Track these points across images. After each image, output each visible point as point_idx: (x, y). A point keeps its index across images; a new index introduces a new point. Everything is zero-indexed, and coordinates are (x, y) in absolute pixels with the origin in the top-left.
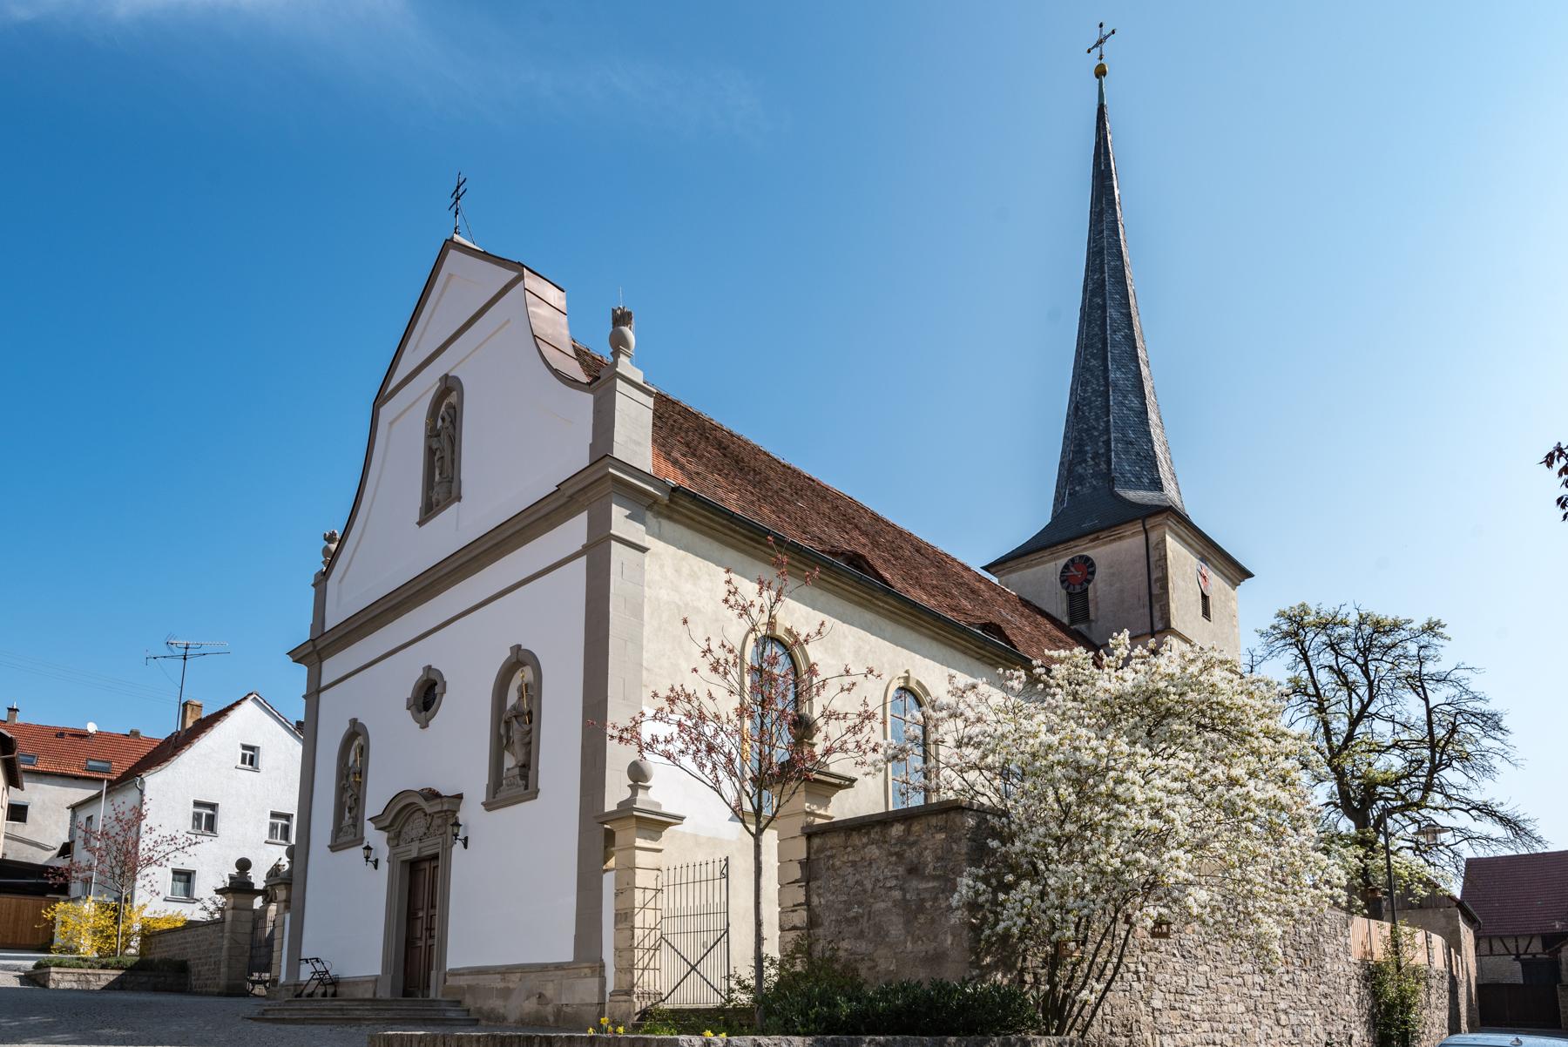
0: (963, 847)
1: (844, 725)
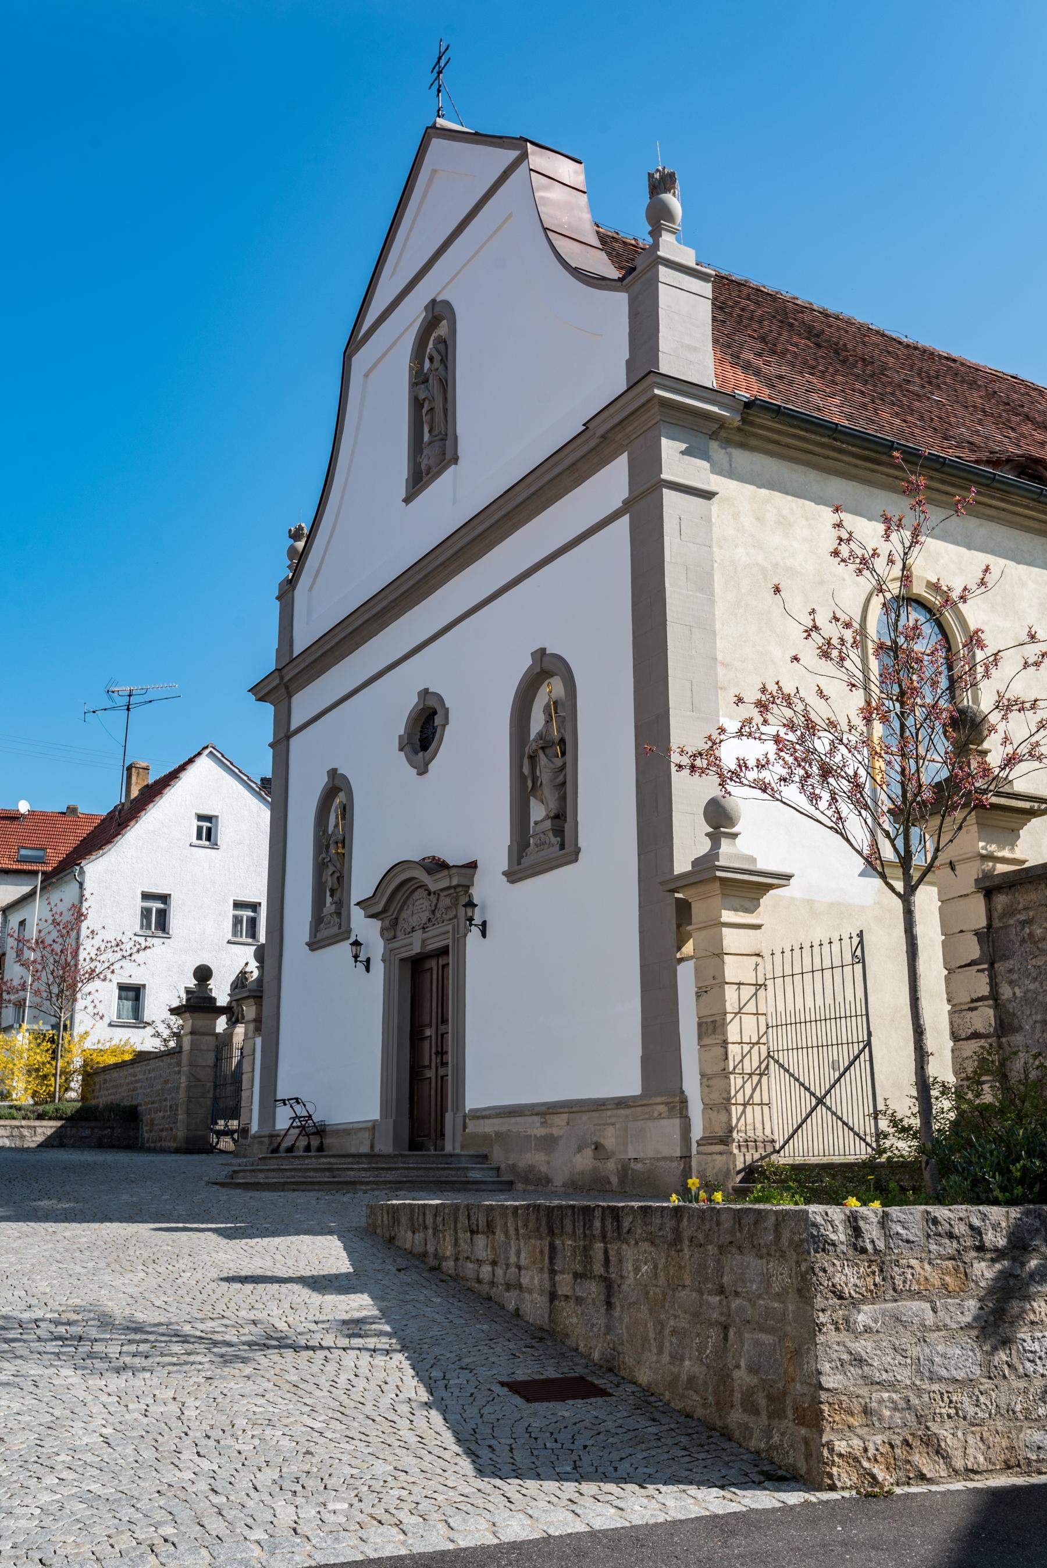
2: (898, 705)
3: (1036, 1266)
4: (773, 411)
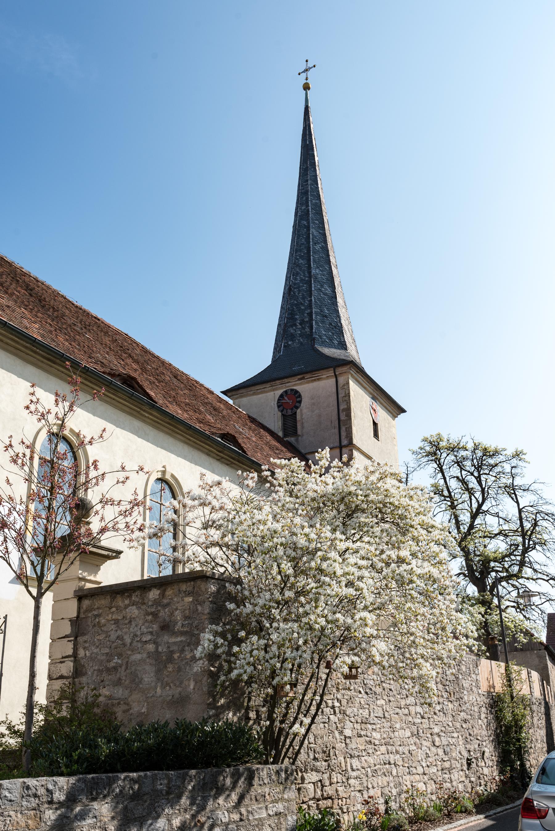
0: (206, 609)
1: (117, 509)
2: (49, 493)
3: (79, 811)
4: (2, 324)
